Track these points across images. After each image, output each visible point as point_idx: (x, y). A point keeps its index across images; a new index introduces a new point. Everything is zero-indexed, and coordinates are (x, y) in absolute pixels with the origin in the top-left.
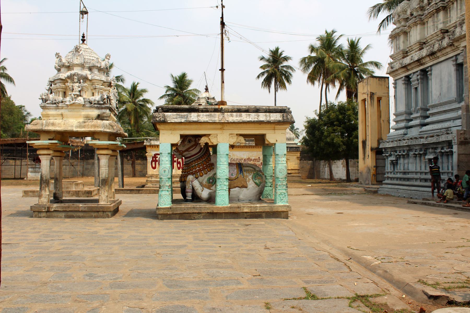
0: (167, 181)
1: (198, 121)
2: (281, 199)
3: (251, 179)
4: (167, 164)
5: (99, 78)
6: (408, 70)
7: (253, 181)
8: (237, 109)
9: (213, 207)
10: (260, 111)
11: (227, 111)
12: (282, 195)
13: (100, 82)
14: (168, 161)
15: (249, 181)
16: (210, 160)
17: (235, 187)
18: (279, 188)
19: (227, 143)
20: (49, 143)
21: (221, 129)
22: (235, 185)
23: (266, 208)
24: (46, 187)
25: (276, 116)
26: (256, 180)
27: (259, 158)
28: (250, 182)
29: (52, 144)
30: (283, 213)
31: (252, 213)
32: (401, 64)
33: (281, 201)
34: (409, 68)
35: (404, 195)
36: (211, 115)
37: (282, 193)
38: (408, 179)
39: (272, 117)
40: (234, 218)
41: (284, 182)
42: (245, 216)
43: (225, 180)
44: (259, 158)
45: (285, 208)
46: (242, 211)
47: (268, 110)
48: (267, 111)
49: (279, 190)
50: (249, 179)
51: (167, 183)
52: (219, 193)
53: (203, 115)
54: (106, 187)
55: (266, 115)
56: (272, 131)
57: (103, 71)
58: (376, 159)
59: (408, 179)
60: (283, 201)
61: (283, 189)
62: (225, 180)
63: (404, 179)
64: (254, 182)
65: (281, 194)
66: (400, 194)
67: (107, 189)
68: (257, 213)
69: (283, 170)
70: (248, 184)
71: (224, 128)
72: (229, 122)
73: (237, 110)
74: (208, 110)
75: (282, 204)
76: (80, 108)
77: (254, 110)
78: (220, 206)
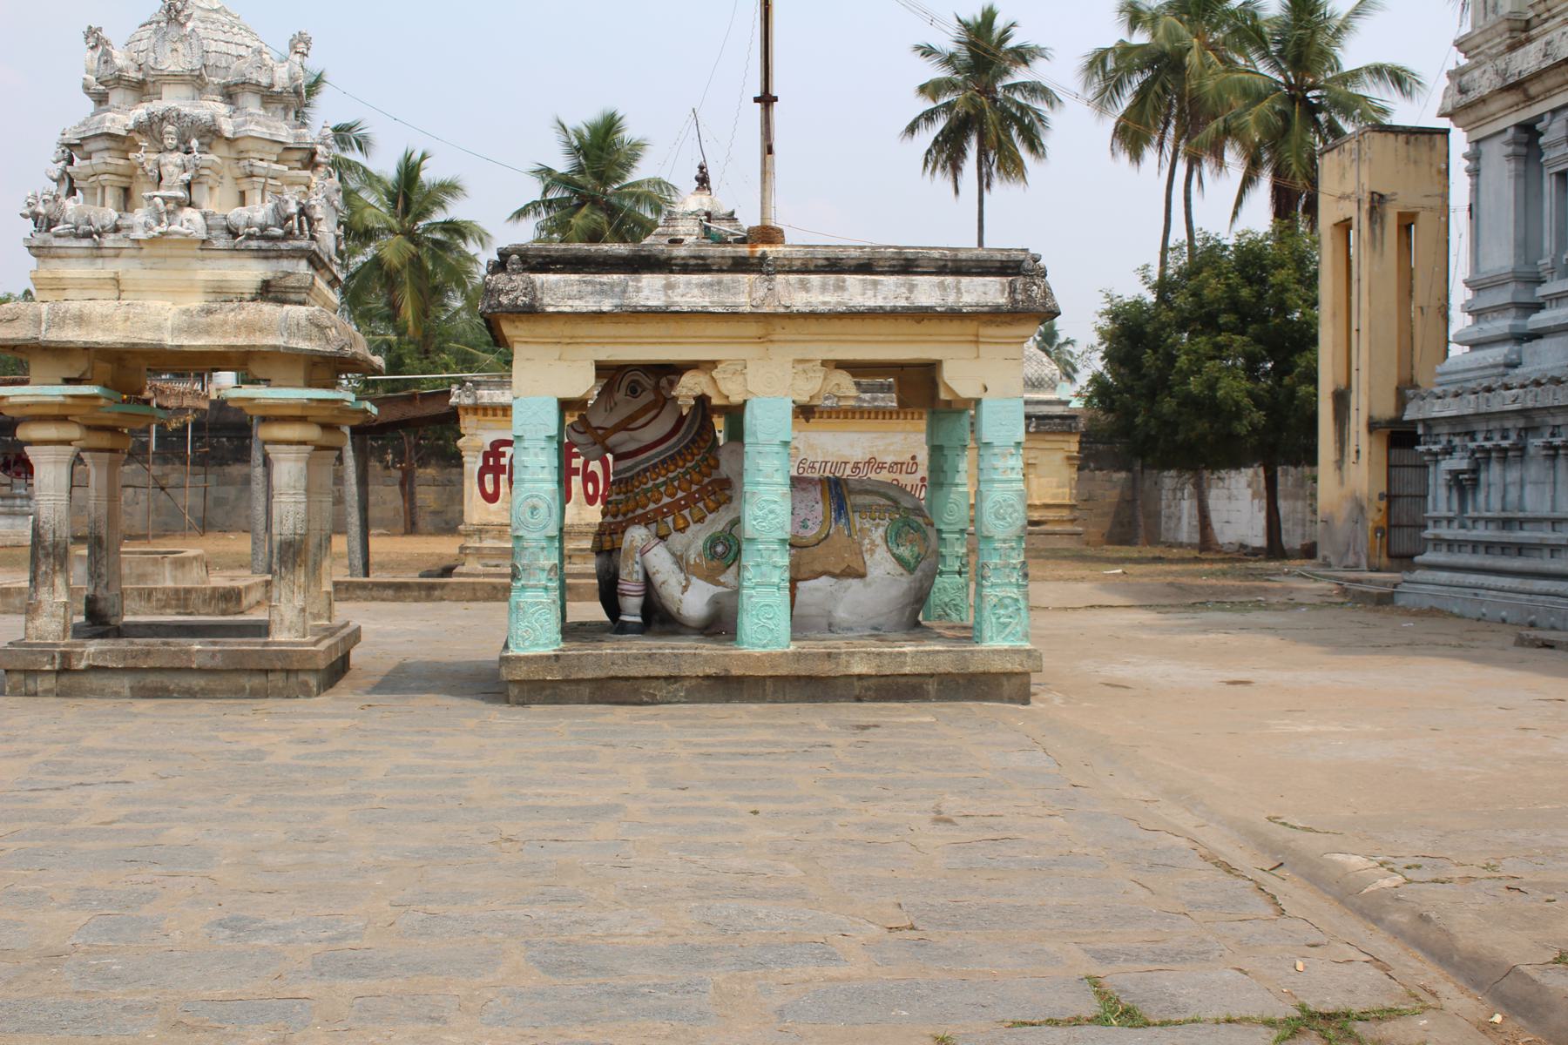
0: (543, 548)
1: (667, 307)
2: (1003, 624)
3: (879, 541)
4: (543, 481)
5: (265, 130)
6: (1530, 100)
7: (890, 550)
8: (827, 259)
9: (727, 655)
10: (917, 266)
11: (787, 269)
12: (1006, 607)
13: (268, 146)
14: (546, 470)
15: (872, 552)
16: (717, 466)
17: (817, 575)
18: (992, 579)
19: (786, 395)
20: (64, 396)
21: (762, 340)
22: (818, 567)
23: (940, 658)
24: (54, 572)
25: (981, 289)
26: (902, 548)
27: (914, 458)
28: (877, 556)
29: (78, 401)
30: (1008, 680)
31: (883, 679)
32: (1502, 74)
33: (999, 633)
34: (1534, 89)
35: (1504, 614)
36: (720, 283)
37: (1007, 601)
38: (1521, 549)
39: (968, 292)
40: (812, 699)
41: (1014, 554)
42: (857, 692)
43: (776, 547)
44: (914, 458)
45: (1017, 659)
46: (841, 671)
47: (950, 264)
48: (945, 266)
49: (993, 585)
50: (873, 543)
51: (542, 557)
52: (752, 597)
53: (688, 283)
54: (297, 573)
55: (942, 283)
56: (967, 351)
57: (281, 101)
58: (1390, 466)
59: (1521, 549)
60: (1008, 630)
61: (1011, 584)
62: (776, 547)
63: (1505, 548)
64: (894, 555)
65: (1001, 604)
66: (1484, 610)
67: (303, 579)
68: (904, 680)
69: (1012, 506)
70: (868, 563)
71: (775, 338)
72: (792, 312)
73: (825, 263)
74: (708, 262)
75: (1006, 645)
76: (190, 253)
77: (894, 262)
78: (758, 650)
